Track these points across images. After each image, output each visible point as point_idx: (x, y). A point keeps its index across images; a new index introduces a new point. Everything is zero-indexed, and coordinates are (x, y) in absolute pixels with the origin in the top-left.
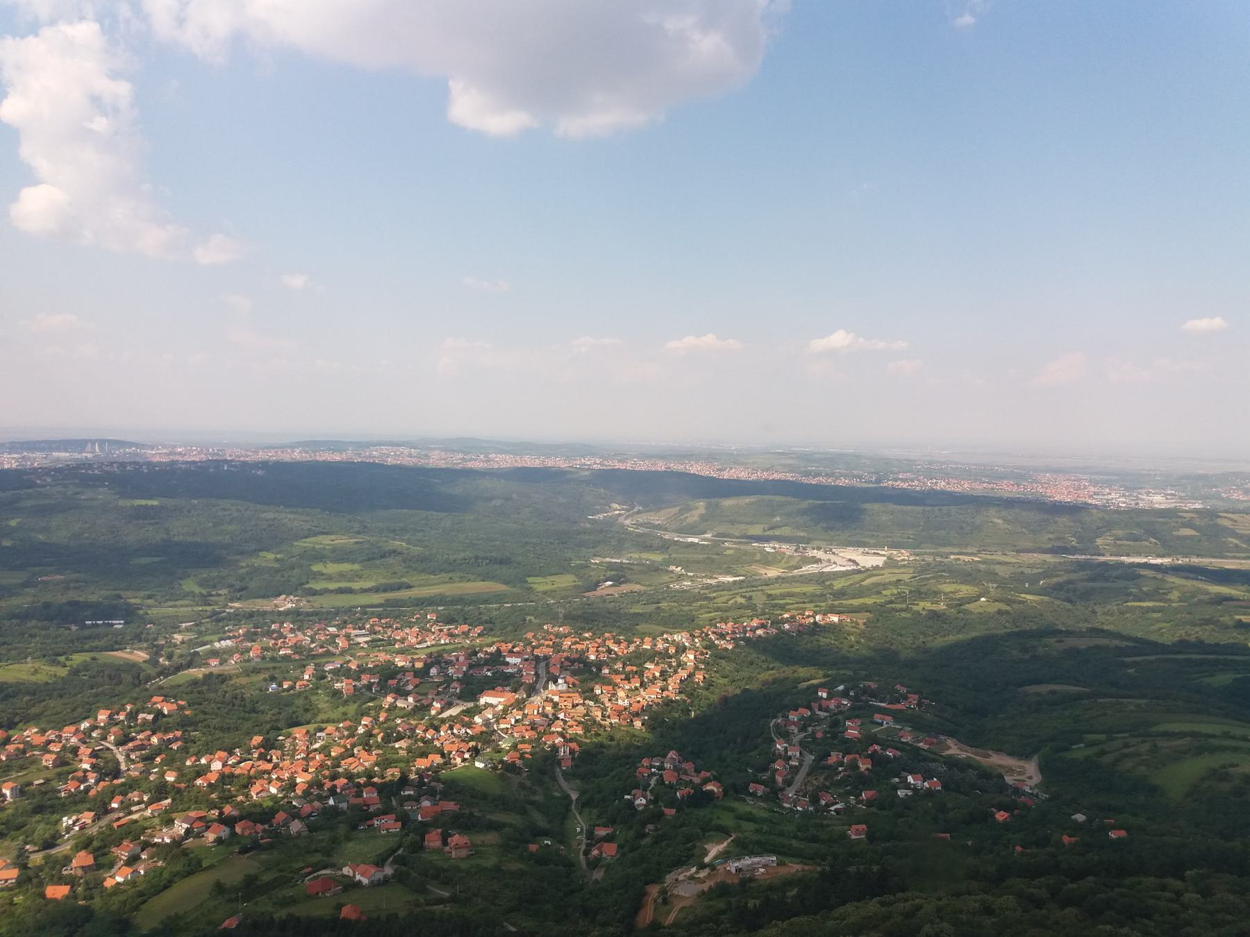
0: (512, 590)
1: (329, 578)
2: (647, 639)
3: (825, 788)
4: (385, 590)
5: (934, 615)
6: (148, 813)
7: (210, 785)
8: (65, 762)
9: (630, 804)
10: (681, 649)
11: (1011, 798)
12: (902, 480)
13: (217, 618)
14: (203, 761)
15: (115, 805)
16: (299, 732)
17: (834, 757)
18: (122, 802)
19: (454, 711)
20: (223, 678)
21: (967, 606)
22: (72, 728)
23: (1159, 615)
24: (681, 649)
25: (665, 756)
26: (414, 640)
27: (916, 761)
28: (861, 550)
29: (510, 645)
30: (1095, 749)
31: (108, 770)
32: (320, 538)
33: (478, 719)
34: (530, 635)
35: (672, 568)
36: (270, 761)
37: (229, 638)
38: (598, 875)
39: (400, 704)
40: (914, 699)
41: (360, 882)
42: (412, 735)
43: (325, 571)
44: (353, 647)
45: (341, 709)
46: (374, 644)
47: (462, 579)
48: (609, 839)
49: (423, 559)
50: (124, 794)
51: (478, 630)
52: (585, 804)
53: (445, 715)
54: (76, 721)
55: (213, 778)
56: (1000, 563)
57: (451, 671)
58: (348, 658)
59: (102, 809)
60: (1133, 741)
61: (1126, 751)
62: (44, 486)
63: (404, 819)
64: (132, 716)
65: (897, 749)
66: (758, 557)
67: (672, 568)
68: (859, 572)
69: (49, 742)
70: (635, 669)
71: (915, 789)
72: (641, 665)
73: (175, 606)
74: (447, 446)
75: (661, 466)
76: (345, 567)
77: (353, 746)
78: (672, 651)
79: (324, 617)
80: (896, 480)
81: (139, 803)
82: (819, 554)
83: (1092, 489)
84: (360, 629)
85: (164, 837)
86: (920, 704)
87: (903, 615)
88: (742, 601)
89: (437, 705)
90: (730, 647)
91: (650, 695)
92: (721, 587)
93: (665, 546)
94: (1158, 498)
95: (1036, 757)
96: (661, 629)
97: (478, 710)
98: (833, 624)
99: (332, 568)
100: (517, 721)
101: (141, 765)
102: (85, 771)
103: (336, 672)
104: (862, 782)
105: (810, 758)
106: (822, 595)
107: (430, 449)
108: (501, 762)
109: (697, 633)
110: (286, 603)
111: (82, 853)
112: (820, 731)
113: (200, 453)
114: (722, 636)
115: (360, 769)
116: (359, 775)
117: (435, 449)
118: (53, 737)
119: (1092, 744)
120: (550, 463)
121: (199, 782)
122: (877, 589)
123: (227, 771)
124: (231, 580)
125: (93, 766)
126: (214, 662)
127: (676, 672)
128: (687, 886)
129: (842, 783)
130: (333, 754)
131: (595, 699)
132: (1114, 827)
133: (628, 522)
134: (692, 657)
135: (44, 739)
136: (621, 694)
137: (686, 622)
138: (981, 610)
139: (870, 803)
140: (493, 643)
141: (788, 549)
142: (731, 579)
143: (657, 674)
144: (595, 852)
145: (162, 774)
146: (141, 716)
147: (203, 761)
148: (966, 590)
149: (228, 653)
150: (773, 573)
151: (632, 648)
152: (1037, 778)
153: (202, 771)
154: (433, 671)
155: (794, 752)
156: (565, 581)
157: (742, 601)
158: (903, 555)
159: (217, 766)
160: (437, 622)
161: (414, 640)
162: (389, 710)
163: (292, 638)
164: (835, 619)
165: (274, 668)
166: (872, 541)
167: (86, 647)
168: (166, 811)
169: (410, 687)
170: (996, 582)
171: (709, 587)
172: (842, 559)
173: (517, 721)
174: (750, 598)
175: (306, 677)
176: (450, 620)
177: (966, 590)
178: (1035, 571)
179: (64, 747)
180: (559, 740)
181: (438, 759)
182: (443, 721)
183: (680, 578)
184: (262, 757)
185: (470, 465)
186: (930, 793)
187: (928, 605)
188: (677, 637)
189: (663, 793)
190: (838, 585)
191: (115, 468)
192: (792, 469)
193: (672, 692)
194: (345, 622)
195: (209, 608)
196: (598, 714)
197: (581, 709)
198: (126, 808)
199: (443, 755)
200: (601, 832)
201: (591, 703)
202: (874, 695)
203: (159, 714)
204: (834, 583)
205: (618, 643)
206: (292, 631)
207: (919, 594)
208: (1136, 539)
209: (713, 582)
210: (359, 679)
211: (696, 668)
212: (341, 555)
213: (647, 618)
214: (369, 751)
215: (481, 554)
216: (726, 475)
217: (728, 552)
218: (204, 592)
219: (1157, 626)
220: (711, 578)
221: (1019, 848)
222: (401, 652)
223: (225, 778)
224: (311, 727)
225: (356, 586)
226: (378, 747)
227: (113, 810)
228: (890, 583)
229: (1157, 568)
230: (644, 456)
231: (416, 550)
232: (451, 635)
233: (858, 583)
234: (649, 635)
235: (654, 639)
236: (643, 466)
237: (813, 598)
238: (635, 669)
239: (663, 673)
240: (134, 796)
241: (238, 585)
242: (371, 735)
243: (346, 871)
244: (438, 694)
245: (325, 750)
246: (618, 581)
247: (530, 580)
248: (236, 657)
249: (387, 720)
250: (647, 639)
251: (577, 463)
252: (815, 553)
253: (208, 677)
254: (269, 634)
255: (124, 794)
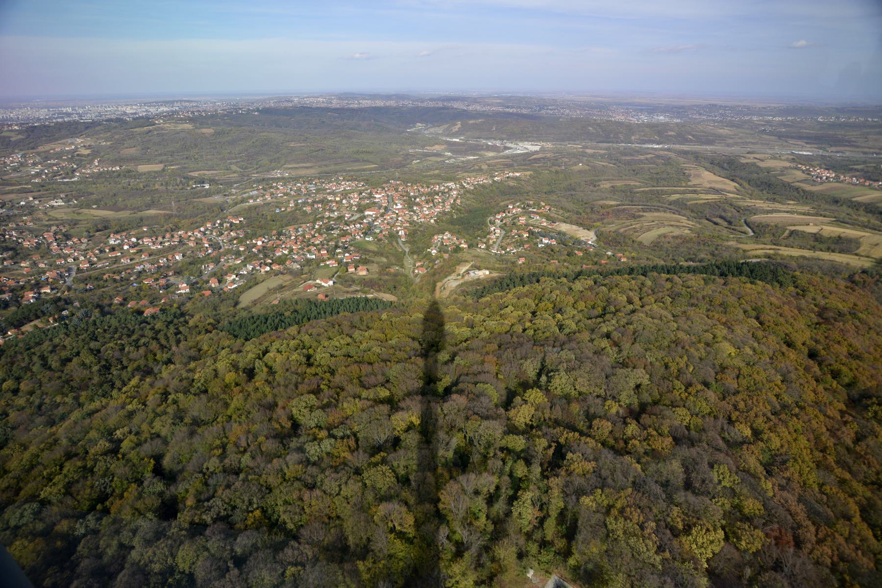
3: (508, 244)
9: (430, 253)
16: (291, 228)
27: (545, 234)
31: (215, 246)
48: (422, 266)
52: (412, 253)
59: (217, 261)
63: (340, 262)
64: (221, 225)
74: (341, 97)
79: (296, 179)
94: (662, 118)
97: (365, 217)
103: (257, 197)
112: (508, 221)
126: (251, 201)
131: (414, 212)
149: (256, 198)
152: (595, 238)
158: (549, 145)
160: (344, 180)
171: (463, 162)
182: (351, 222)
183: (449, 158)
184: (277, 239)
185: (352, 106)
189: (442, 249)
192: (500, 105)
193: (448, 209)
196: (415, 218)
198: (227, 261)
200: (418, 264)
203: (232, 224)
205: (423, 187)
222: (329, 194)
230: (431, 100)
233: (525, 160)
236: (431, 104)
243: (318, 281)
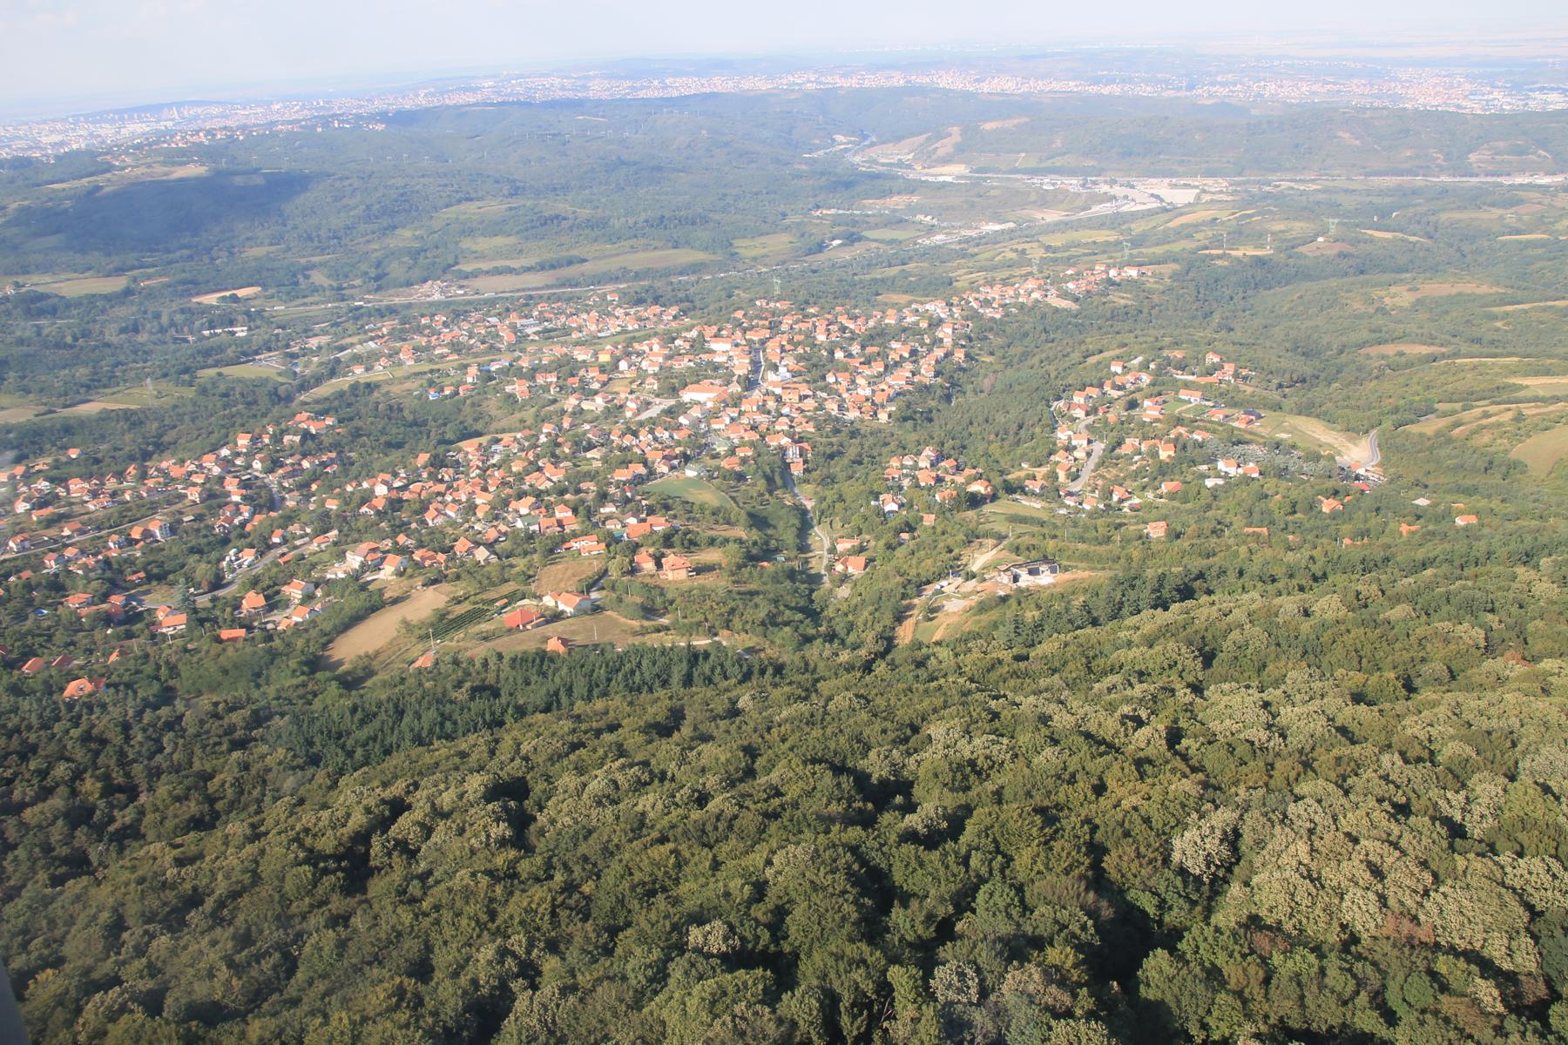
0: (713, 257)
1: (482, 257)
2: (890, 312)
4: (553, 267)
5: (1260, 262)
6: (314, 547)
7: (378, 513)
8: (214, 497)
10: (936, 323)
11: (1341, 481)
12: (1223, 85)
13: (357, 314)
14: (365, 485)
15: (276, 540)
16: (469, 446)
17: (1130, 443)
18: (284, 537)
19: (653, 412)
20: (370, 387)
21: (1301, 249)
22: (212, 457)
23: (1540, 251)
24: (936, 323)
25: (919, 453)
26: (593, 328)
28: (1167, 181)
29: (714, 329)
30: (1450, 419)
32: (463, 207)
33: (682, 420)
34: (739, 314)
35: (920, 217)
36: (442, 481)
37: (372, 339)
38: (844, 592)
39: (586, 406)
40: (1229, 368)
41: (563, 612)
42: (606, 443)
43: (474, 247)
44: (521, 338)
45: (518, 415)
46: (547, 335)
47: (646, 248)
49: (592, 224)
50: (284, 527)
51: (673, 311)
53: (644, 416)
54: (214, 449)
55: (380, 504)
56: (1346, 191)
57: (645, 365)
58: (517, 354)
59: (265, 547)
60: (1493, 409)
61: (1485, 422)
62: (123, 169)
64: (277, 438)
65: (1207, 430)
66: (1033, 197)
67: (920, 217)
68: (1165, 210)
69: (190, 474)
70: (876, 349)
71: (1226, 476)
72: (884, 346)
73: (305, 304)
75: (898, 80)
76: (499, 241)
77: (538, 457)
78: (924, 325)
80: (1213, 84)
81: (302, 537)
82: (1117, 190)
83: (1467, 86)
84: (526, 317)
85: (337, 572)
86: (1236, 375)
87: (1219, 262)
88: (1014, 255)
89: (632, 405)
90: (998, 316)
91: (898, 380)
92: (981, 240)
93: (912, 187)
95: (1374, 432)
96: (908, 297)
98: (1130, 281)
99: (483, 244)
100: (732, 419)
101: (296, 493)
102: (237, 504)
103: (504, 372)
104: (1164, 471)
105: (1099, 447)
106: (1118, 243)
107: (588, 78)
108: (718, 468)
109: (955, 300)
110: (433, 292)
111: (252, 594)
113: (303, 108)
114: (987, 303)
115: (549, 485)
116: (547, 492)
117: (595, 77)
118: (192, 468)
119: (1445, 415)
120: (746, 85)
121: (364, 509)
122: (1186, 232)
123: (394, 495)
124: (364, 267)
125: (245, 498)
126: (359, 370)
127: (930, 351)
128: (955, 601)
129: (1135, 475)
130: (514, 469)
132: (1460, 513)
133: (857, 159)
134: (950, 331)
135: (184, 470)
136: (860, 381)
137: (941, 287)
138: (1318, 253)
139: (1172, 496)
140: (693, 326)
141: (1073, 184)
142: (998, 227)
143: (906, 355)
144: (839, 567)
145: (323, 502)
146: (287, 439)
147: (365, 485)
148: (1299, 227)
150: (1052, 216)
151: (871, 323)
153: (367, 498)
154: (623, 365)
155: (1080, 442)
156: (780, 242)
157: (1014, 255)
159: (381, 490)
161: (593, 328)
162: (574, 413)
163: (447, 335)
164: (1133, 273)
165: (432, 371)
166: (1181, 169)
167: (210, 361)
168: (335, 544)
169: (596, 386)
170: (1337, 216)
171: (968, 241)
172: (1144, 195)
173: (732, 419)
174: (1024, 251)
175: (470, 380)
176: (639, 302)
177: (1299, 227)
178: (1387, 200)
179: (208, 479)
180: (785, 441)
181: (641, 470)
182: (641, 424)
186: (1247, 480)
187: (1252, 252)
188: (930, 307)
190: (1138, 228)
191: (202, 138)
194: (508, 310)
195: (342, 304)
196: (832, 407)
197: (810, 404)
199: (645, 463)
201: (824, 395)
202: (1182, 366)
203: (306, 435)
204: (1133, 226)
205: (854, 318)
206: (445, 325)
207: (1239, 234)
208: (1521, 152)
209: (973, 233)
210: (533, 378)
211: (955, 344)
212: (494, 228)
213: (889, 284)
214: (555, 464)
215: (667, 214)
216: (985, 88)
217: (992, 193)
218: (335, 284)
219: (1540, 264)
220: (970, 228)
221: (1347, 541)
223: (395, 504)
224: (484, 440)
225: (515, 264)
226: (566, 458)
227: (276, 546)
228: (1204, 223)
229: (1544, 189)
231: (585, 213)
232: (640, 319)
234: (894, 305)
235: (900, 310)
237: (1107, 248)
238: (876, 349)
239: (914, 352)
240: (295, 528)
241: (373, 272)
242: (558, 445)
243: (548, 601)
244: (632, 392)
245: (506, 462)
246: (851, 239)
247: (736, 243)
248: (383, 361)
249: (572, 426)
250: (890, 312)
251: (785, 81)
252: (1105, 188)
253: (355, 387)
254: (419, 330)
255: (284, 527)
